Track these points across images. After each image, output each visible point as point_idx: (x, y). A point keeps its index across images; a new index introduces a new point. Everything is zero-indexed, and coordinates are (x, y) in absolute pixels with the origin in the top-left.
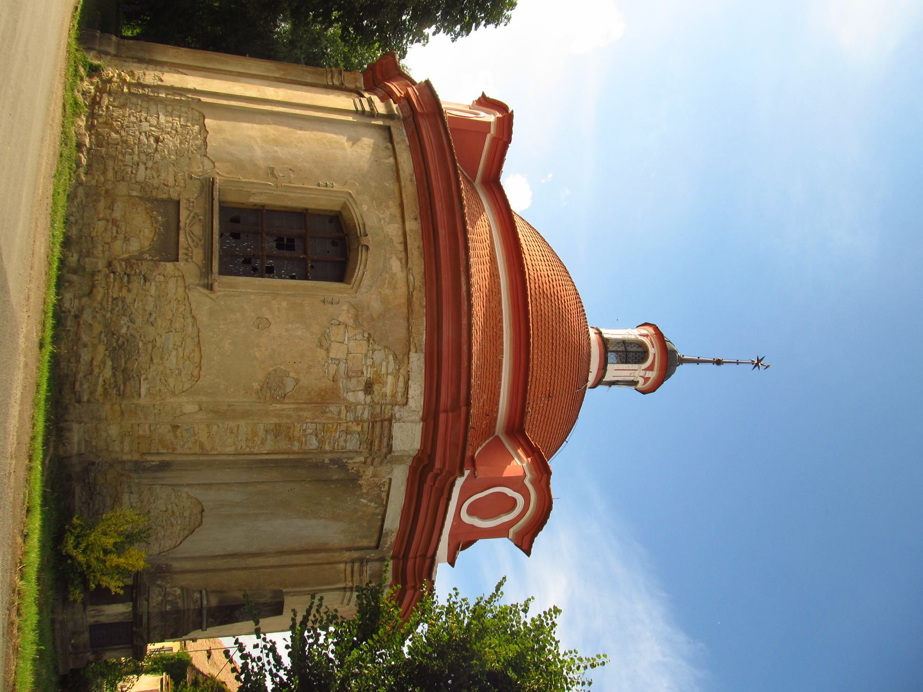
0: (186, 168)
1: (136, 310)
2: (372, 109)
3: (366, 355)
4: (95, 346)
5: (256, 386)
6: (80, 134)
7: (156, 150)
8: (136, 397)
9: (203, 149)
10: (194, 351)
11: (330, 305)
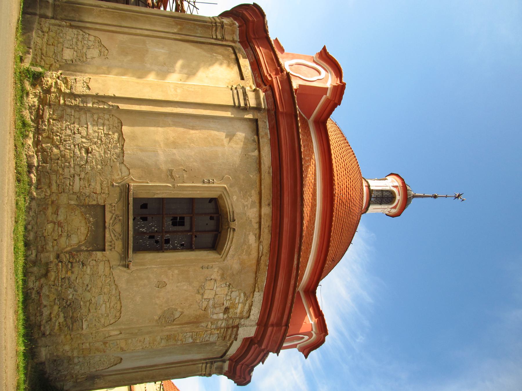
0: (109, 176)
1: (78, 284)
2: (246, 104)
3: (227, 295)
4: (52, 307)
5: (156, 318)
7: (87, 162)
8: (80, 330)
10: (116, 303)
11: (206, 269)
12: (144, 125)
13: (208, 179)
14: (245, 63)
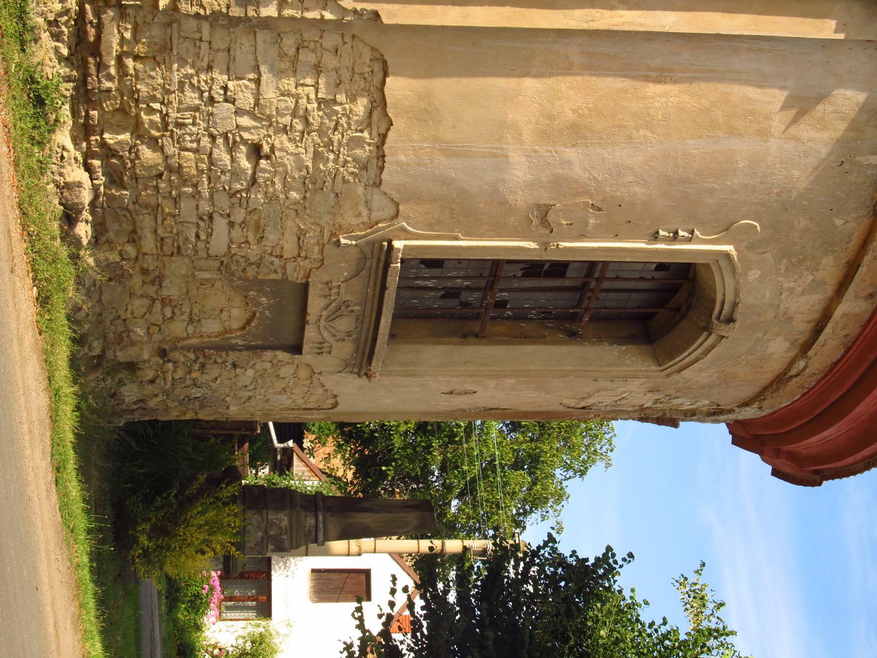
0: (327, 218)
6: (68, 186)
7: (254, 181)
9: (373, 172)
12: (472, 70)
13: (673, 228)
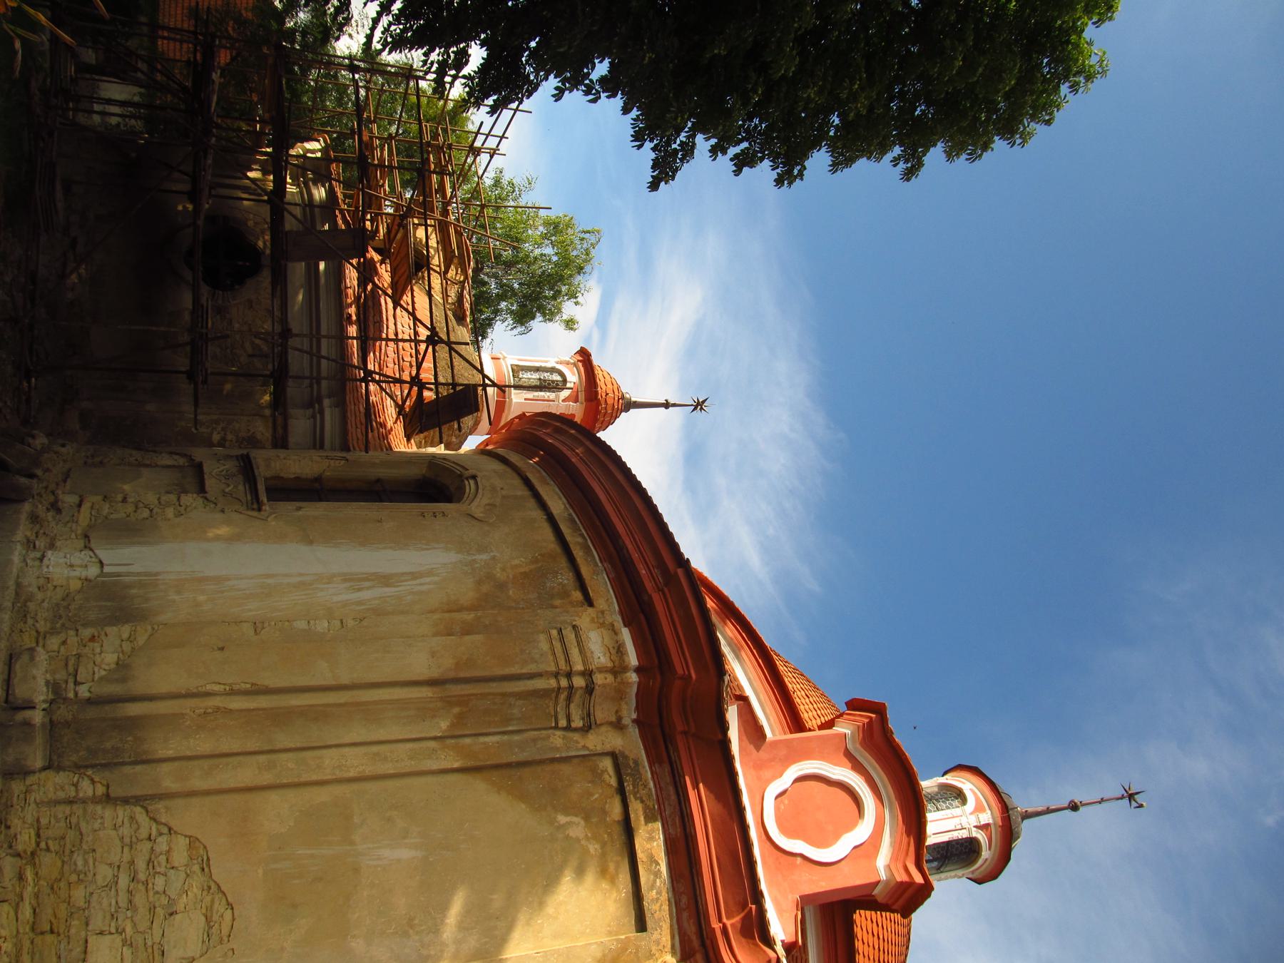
14: (651, 842)
